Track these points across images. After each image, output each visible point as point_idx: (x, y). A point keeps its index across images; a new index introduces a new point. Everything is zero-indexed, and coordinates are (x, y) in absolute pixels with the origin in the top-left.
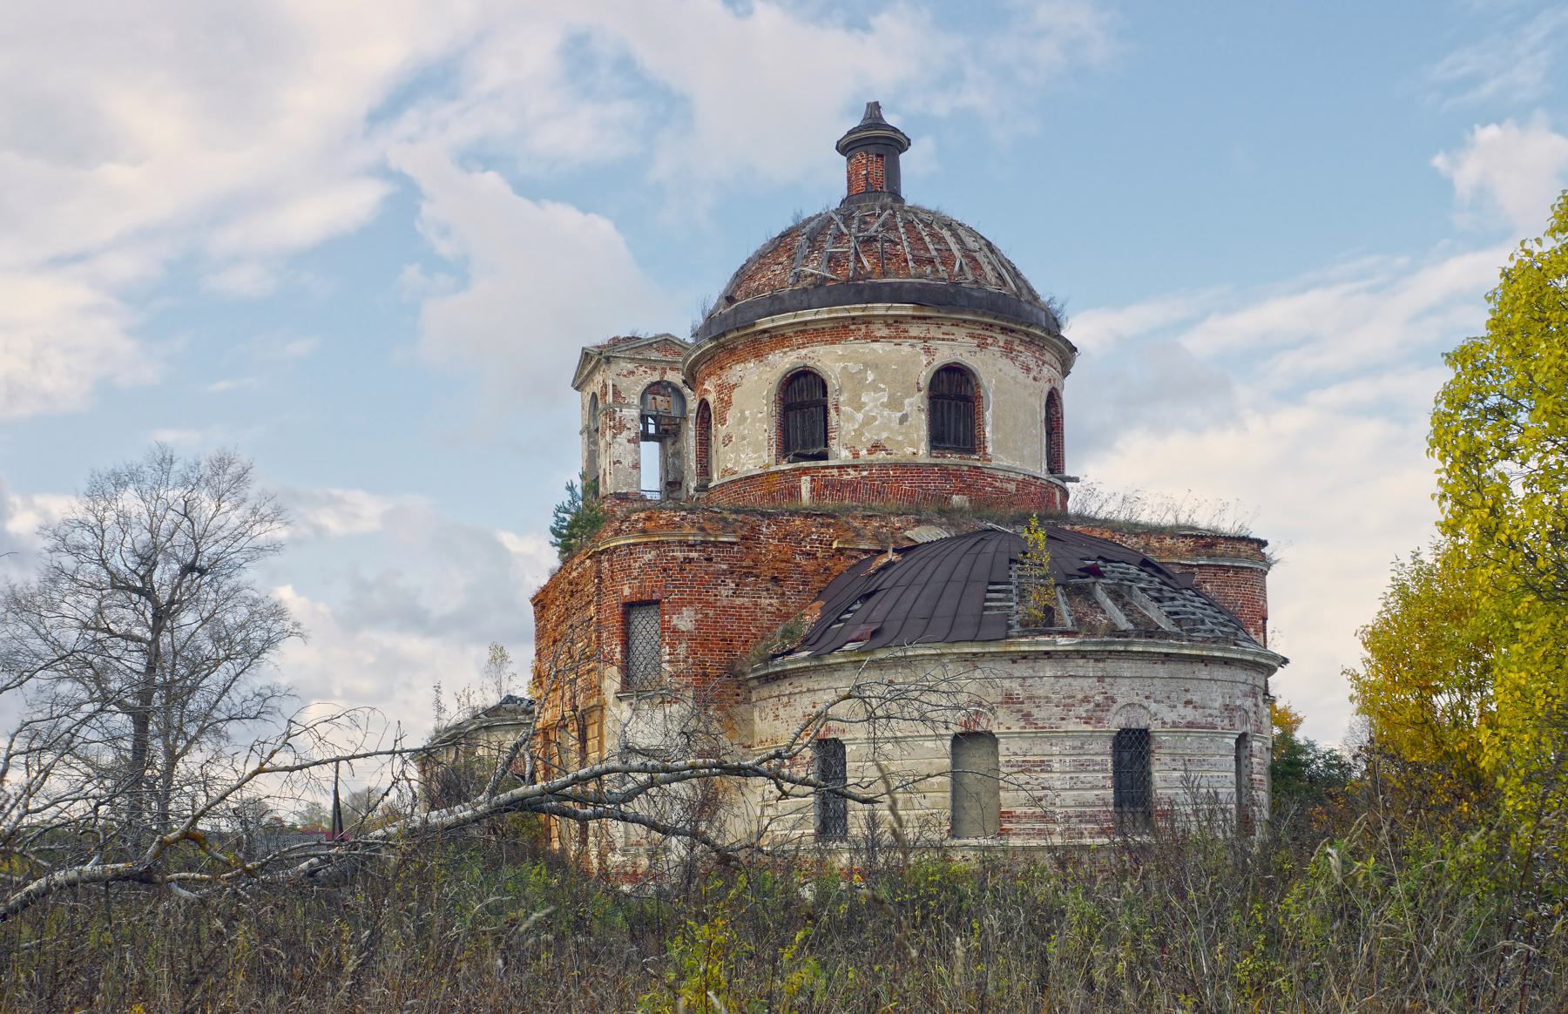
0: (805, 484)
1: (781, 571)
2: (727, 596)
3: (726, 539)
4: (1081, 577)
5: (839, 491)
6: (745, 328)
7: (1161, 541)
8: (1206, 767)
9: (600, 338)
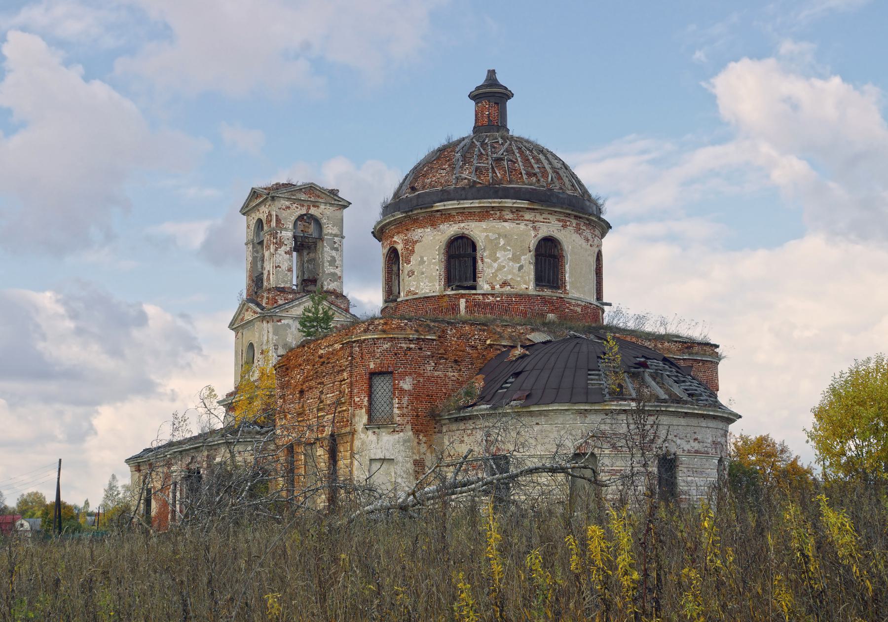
0: (463, 303)
1: (460, 356)
2: (430, 371)
3: (430, 337)
4: (635, 368)
5: (483, 309)
6: (426, 208)
7: (662, 344)
8: (704, 475)
9: (264, 182)
